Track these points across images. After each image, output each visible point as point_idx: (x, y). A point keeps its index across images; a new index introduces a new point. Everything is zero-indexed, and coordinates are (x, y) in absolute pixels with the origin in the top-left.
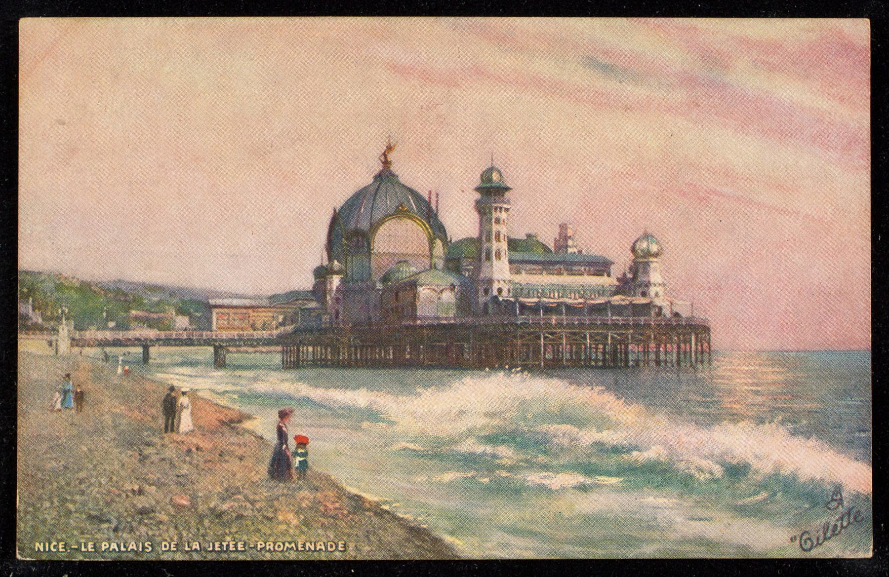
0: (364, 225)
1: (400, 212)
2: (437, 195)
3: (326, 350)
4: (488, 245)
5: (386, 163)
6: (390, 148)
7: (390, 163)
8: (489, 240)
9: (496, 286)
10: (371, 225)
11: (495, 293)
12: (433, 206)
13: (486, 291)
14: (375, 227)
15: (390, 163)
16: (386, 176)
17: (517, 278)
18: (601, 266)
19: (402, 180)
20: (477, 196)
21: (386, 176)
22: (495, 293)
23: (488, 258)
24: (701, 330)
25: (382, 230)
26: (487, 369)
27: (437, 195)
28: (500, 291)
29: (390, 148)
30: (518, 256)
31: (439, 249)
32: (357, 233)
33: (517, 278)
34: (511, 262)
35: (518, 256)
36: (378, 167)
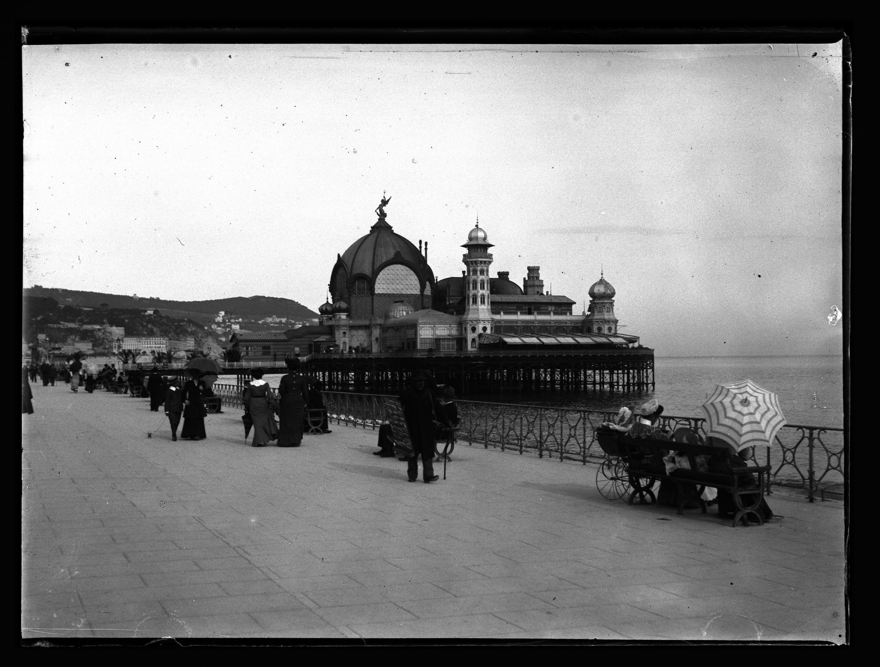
0: (367, 271)
1: (397, 260)
2: (426, 244)
3: (628, 373)
4: (475, 292)
5: (382, 215)
6: (385, 202)
7: (385, 215)
8: (475, 288)
9: (480, 326)
10: (373, 272)
11: (481, 331)
12: (423, 253)
13: (474, 329)
14: (376, 273)
15: (385, 215)
16: (381, 228)
17: (497, 317)
18: (565, 305)
19: (396, 231)
20: (465, 251)
21: (381, 228)
22: (481, 331)
23: (475, 302)
24: (289, 438)
25: (381, 276)
26: (440, 447)
27: (426, 244)
28: (485, 329)
29: (385, 202)
30: (498, 298)
31: (428, 291)
32: (361, 277)
33: (497, 317)
34: (493, 303)
35: (498, 298)
36: (375, 219)
